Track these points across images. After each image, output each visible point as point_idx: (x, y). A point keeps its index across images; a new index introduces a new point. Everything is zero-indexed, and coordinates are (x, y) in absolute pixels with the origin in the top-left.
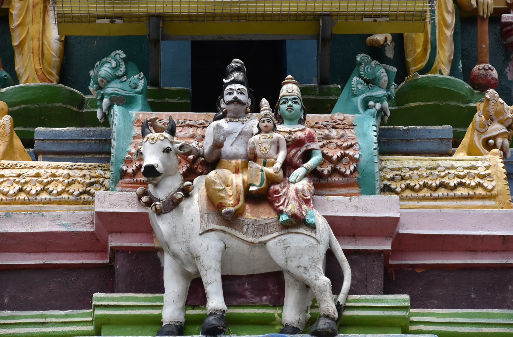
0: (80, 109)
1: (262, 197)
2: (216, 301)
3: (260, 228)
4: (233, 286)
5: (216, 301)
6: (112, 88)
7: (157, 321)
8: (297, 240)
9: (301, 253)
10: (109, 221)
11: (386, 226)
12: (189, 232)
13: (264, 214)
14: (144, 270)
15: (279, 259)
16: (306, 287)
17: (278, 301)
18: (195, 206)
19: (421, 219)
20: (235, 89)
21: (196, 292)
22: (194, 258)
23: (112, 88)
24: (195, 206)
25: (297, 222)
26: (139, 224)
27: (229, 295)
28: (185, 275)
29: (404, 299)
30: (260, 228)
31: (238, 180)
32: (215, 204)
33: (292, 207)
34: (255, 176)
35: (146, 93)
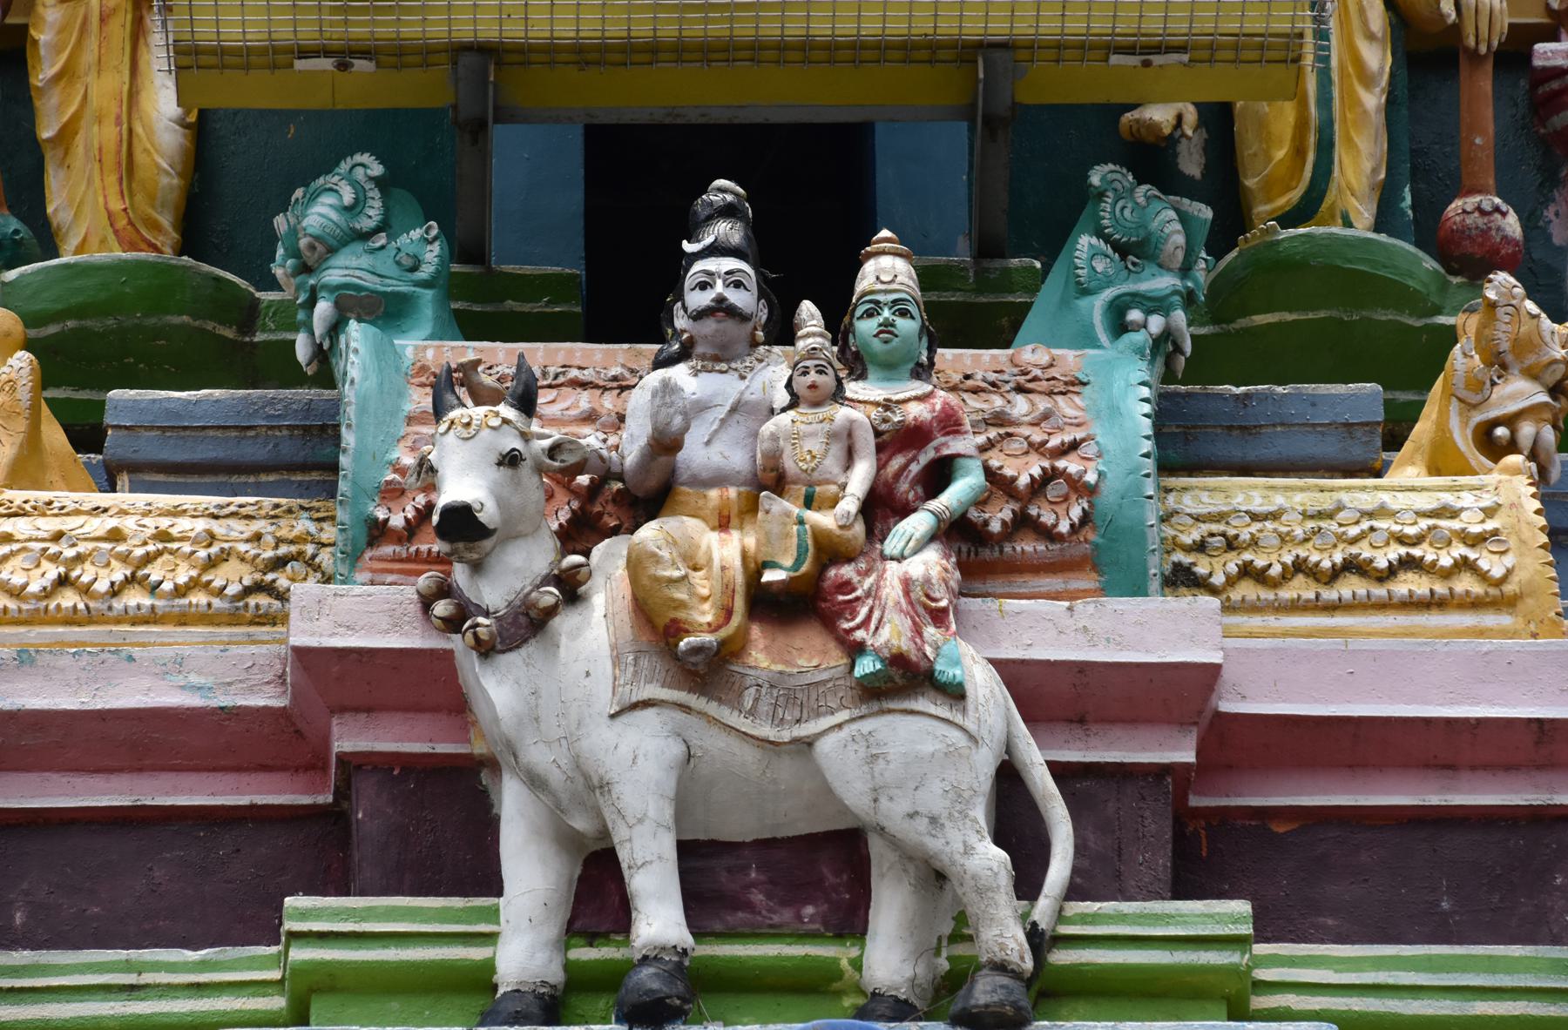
0: (245, 334)
1: (799, 601)
2: (659, 919)
3: (795, 698)
4: (712, 874)
5: (659, 919)
6: (343, 270)
7: (480, 980)
8: (909, 732)
9: (921, 775)
10: (335, 677)
11: (1179, 692)
12: (578, 710)
13: (807, 655)
14: (439, 825)
15: (854, 792)
16: (934, 878)
17: (850, 921)
18: (595, 631)
19: (1287, 670)
20: (718, 272)
21: (598, 892)
22: (593, 787)
23: (343, 270)
24: (595, 631)
25: (907, 679)
26: (425, 684)
27: (700, 902)
28: (567, 840)
29: (1234, 913)
30: (795, 698)
31: (726, 550)
32: (656, 623)
33: (892, 633)
34: (779, 539)
35: (447, 285)
